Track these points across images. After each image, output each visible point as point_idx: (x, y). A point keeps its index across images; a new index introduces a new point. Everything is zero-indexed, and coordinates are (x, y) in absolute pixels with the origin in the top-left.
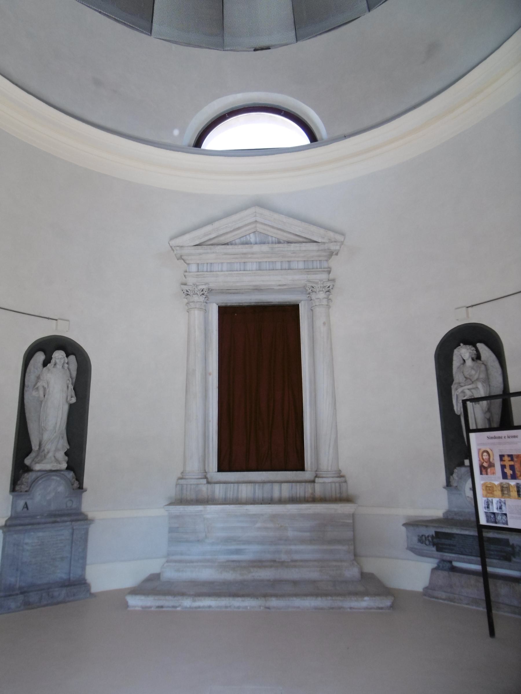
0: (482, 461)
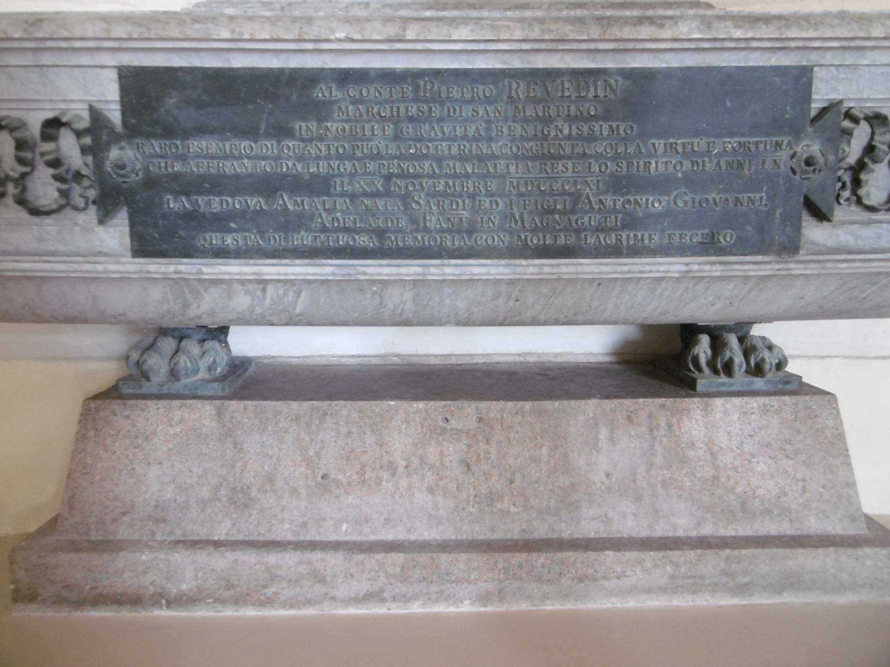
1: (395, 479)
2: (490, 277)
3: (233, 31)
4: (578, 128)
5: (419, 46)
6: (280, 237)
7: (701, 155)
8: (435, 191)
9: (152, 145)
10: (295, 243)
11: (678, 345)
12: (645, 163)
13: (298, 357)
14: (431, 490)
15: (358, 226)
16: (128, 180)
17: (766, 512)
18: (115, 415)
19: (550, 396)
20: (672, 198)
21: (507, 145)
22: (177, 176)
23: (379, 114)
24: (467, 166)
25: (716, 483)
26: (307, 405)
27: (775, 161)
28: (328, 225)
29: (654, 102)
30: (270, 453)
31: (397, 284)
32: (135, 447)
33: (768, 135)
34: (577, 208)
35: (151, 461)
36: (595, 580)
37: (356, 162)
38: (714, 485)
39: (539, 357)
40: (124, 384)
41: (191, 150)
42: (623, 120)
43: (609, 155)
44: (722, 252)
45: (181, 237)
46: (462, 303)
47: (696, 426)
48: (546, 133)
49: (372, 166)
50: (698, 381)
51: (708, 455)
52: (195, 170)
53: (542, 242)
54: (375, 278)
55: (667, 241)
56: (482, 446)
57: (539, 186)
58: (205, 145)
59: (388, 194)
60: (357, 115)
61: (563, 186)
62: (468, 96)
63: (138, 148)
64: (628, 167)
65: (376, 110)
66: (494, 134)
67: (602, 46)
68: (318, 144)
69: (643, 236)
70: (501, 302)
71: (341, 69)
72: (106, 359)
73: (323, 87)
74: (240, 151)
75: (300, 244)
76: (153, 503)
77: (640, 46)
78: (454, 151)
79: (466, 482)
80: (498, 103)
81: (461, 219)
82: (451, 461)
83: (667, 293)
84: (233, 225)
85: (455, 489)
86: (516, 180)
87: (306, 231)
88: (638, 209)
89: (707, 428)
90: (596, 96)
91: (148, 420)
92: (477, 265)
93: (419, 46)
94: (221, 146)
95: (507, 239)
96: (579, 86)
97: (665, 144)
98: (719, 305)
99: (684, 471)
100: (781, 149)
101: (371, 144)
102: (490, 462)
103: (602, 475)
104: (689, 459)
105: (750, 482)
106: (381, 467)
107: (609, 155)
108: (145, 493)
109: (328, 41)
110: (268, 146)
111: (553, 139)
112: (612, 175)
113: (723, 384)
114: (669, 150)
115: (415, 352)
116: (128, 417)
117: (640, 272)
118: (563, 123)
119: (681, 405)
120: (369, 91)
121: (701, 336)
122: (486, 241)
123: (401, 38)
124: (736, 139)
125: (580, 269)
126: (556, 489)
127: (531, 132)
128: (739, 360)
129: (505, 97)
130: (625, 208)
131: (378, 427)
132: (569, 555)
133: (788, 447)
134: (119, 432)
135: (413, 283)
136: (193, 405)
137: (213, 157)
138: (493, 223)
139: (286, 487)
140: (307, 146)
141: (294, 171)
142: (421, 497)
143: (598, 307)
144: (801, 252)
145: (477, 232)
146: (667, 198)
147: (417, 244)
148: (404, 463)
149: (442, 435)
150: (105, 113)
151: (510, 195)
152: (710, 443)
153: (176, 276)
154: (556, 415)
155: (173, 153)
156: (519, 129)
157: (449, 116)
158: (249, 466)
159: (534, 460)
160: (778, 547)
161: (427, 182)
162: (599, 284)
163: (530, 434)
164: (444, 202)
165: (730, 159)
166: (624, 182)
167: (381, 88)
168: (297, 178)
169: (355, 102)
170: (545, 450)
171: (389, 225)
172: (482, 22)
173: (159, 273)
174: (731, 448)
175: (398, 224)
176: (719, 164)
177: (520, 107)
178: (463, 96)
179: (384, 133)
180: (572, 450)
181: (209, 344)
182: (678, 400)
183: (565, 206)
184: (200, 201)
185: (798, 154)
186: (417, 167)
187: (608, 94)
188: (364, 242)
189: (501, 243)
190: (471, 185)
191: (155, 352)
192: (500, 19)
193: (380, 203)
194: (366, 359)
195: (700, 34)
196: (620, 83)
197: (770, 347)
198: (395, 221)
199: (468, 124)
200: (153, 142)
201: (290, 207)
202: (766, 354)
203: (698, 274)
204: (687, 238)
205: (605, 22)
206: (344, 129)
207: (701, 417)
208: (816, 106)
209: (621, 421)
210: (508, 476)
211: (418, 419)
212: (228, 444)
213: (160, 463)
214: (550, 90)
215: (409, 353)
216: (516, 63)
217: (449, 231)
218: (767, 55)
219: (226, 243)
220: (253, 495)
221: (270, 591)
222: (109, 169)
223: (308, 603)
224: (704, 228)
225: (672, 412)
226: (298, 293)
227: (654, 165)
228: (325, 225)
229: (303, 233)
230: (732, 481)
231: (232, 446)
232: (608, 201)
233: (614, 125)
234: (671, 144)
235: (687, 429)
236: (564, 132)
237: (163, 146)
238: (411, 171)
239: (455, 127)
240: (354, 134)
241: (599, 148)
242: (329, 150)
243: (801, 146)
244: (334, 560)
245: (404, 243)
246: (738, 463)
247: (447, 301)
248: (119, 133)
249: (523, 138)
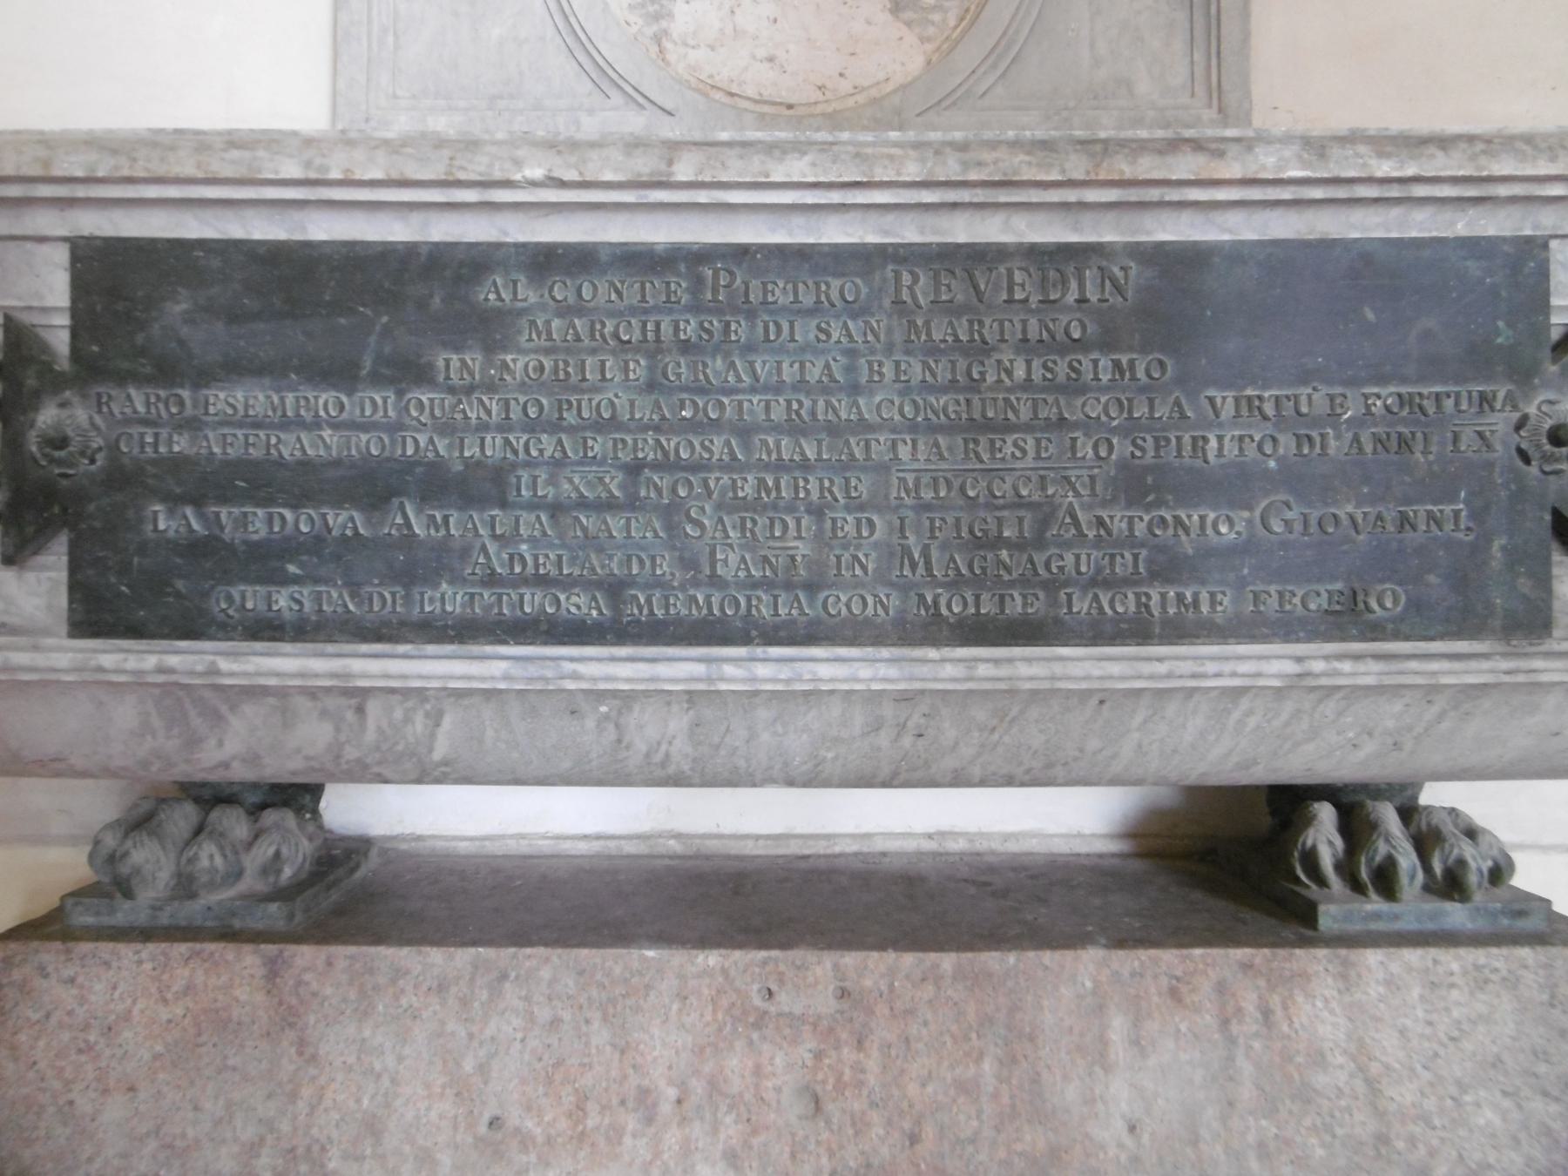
1: (652, 1130)
2: (858, 687)
3: (308, 164)
4: (1045, 366)
5: (703, 197)
6: (393, 595)
7: (1316, 422)
8: (736, 498)
9: (129, 397)
10: (427, 609)
11: (1265, 821)
12: (1194, 439)
13: (471, 839)
15: (565, 572)
16: (71, 472)
18: (46, 976)
19: (994, 938)
20: (1257, 513)
21: (893, 403)
22: (177, 464)
23: (616, 336)
24: (805, 445)
25: (1383, 1151)
26: (464, 956)
27: (1480, 434)
28: (499, 570)
29: (1209, 313)
30: (378, 1066)
31: (652, 700)
32: (80, 1051)
33: (1460, 379)
34: (1048, 534)
35: (112, 1083)
37: (564, 437)
38: (1379, 1155)
39: (971, 841)
40: (76, 904)
41: (212, 410)
42: (1144, 350)
43: (1115, 423)
44: (1375, 631)
45: (178, 595)
46: (798, 738)
47: (1326, 1014)
48: (976, 376)
49: (598, 446)
50: (1322, 908)
51: (1360, 1086)
52: (216, 450)
53: (973, 610)
54: (602, 686)
55: (1251, 608)
56: (848, 1054)
57: (962, 489)
58: (242, 399)
59: (632, 504)
60: (569, 338)
61: (1015, 489)
62: (808, 300)
63: (99, 404)
64: (1157, 448)
65: (609, 328)
66: (863, 380)
67: (1092, 196)
68: (485, 398)
69: (1196, 596)
70: (884, 739)
71: (537, 244)
72: (72, 840)
73: (499, 281)
74: (317, 412)
75: (438, 611)
77: (1174, 195)
78: (778, 414)
79: (813, 1140)
80: (873, 315)
81: (793, 558)
82: (778, 1090)
83: (1252, 722)
84: (292, 569)
85: (786, 1156)
86: (913, 475)
87: (451, 583)
88: (1184, 537)
89: (1350, 1019)
90: (1082, 300)
91: (114, 988)
92: (828, 660)
93: (703, 197)
94: (276, 399)
95: (894, 602)
96: (1044, 279)
97: (1237, 399)
98: (1369, 748)
99: (1307, 1122)
100: (1492, 409)
102: (865, 1092)
103: (1120, 1126)
104: (1315, 1090)
105: (1465, 1154)
106: (623, 1103)
107: (1115, 423)
108: (90, 1160)
109: (507, 184)
110: (378, 401)
111: (990, 389)
112: (1123, 465)
113: (1377, 916)
114: (1245, 412)
115: (715, 830)
116: (72, 980)
117: (1194, 676)
118: (1012, 357)
119: (1288, 965)
120: (595, 288)
121: (1316, 805)
122: (848, 606)
123: (664, 179)
124: (1392, 389)
125: (1058, 669)
126: (1016, 1160)
127: (943, 373)
128: (1407, 860)
129: (887, 303)
130: (1155, 536)
131: (619, 1008)
133: (1542, 1068)
134: (48, 1016)
135: (686, 697)
136: (217, 955)
137: (257, 425)
138: (864, 568)
139: (407, 1149)
140: (460, 402)
141: (430, 455)
143: (1101, 750)
144: (1556, 633)
145: (829, 587)
146: (1246, 514)
147: (694, 612)
148: (672, 1093)
149: (761, 1029)
150: (43, 333)
151: (898, 507)
152: (1360, 1054)
153: (161, 679)
154: (1010, 984)
155: (172, 415)
156: (918, 368)
157: (767, 340)
158: (329, 1094)
159: (967, 1088)
161: (718, 479)
162: (1102, 702)
163: (954, 1028)
164: (754, 522)
165: (1380, 430)
166: (1150, 480)
167: (623, 283)
168: (436, 468)
169: (564, 311)
171: (635, 572)
172: (835, 148)
173: (124, 672)
174: (1413, 1070)
175: (654, 569)
176: (1358, 442)
177: (920, 322)
178: (796, 301)
179: (627, 375)
180: (1049, 1067)
181: (270, 817)
182: (1281, 952)
183: (1021, 531)
184: (223, 517)
185: (1532, 421)
186: (698, 447)
187: (1107, 296)
188: (579, 608)
189: (880, 611)
190: (813, 485)
191: (152, 833)
192: (873, 144)
193: (615, 523)
194: (612, 844)
195: (1303, 169)
196: (1133, 273)
197: (1472, 833)
198: (648, 563)
199: (808, 356)
200: (133, 392)
201: (417, 531)
202: (1467, 850)
203: (1324, 681)
204: (1297, 600)
205: (1098, 148)
206: (541, 368)
207: (1335, 993)
209: (1156, 999)
210: (907, 1125)
211: (706, 991)
212: (285, 1043)
213: (132, 1089)
214: (982, 287)
215: (701, 831)
216: (910, 232)
217: (766, 584)
218: (1447, 214)
219: (275, 608)
220: (332, 1165)
222: (34, 449)
224: (1334, 579)
225: (1269, 981)
226: (436, 718)
227: (1213, 443)
228: (493, 570)
229: (444, 585)
230: (1422, 1150)
231: (293, 1050)
232: (1116, 520)
233: (1124, 360)
234: (1249, 399)
235: (1305, 1020)
236: (1015, 373)
237: (153, 400)
239: (779, 363)
240: (562, 375)
241: (1093, 409)
242: (507, 410)
243: (1536, 402)
245: (667, 612)
246: (1430, 1104)
247: (765, 737)
248: (62, 374)
249: (925, 386)
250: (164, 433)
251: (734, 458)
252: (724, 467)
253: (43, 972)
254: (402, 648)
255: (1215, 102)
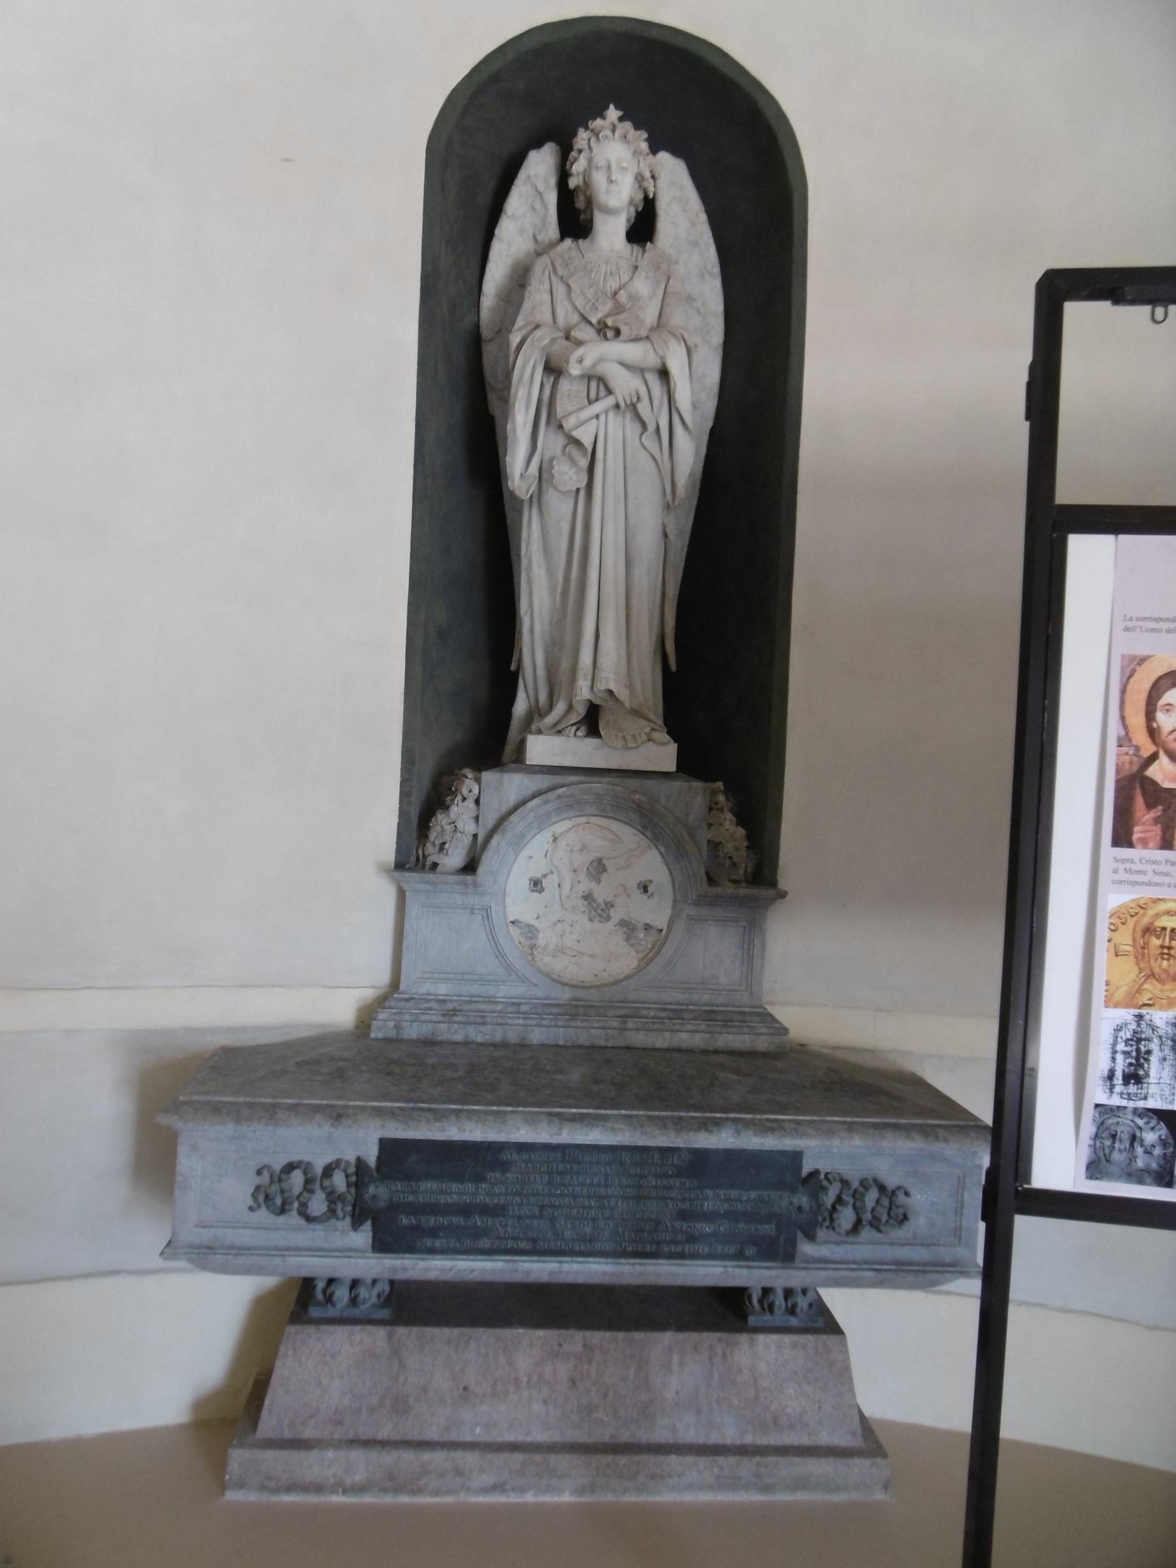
0: (1148, 748)
14: (545, 1402)
17: (792, 1426)
36: (662, 1477)
44: (747, 1259)
49: (533, 1200)
59: (541, 1217)
62: (595, 1160)
76: (334, 1409)
78: (585, 1192)
90: (673, 1164)
101: (533, 1187)
110: (470, 1187)
132: (644, 1458)
134: (311, 1351)
137: (433, 1193)
142: (537, 1407)
144: (797, 1260)
160: (794, 1455)
170: (632, 1371)
182: (732, 1335)
193: (536, 1222)
200: (398, 1183)
208: (806, 1170)
217: (578, 1241)
221: (421, 1483)
223: (449, 1492)
238: (557, 1203)
244: (470, 1459)
249: (627, 1186)
250: (406, 1195)
251: (571, 1205)
252: (568, 1207)
253: (309, 1335)
254: (471, 1257)
255: (749, 990)
